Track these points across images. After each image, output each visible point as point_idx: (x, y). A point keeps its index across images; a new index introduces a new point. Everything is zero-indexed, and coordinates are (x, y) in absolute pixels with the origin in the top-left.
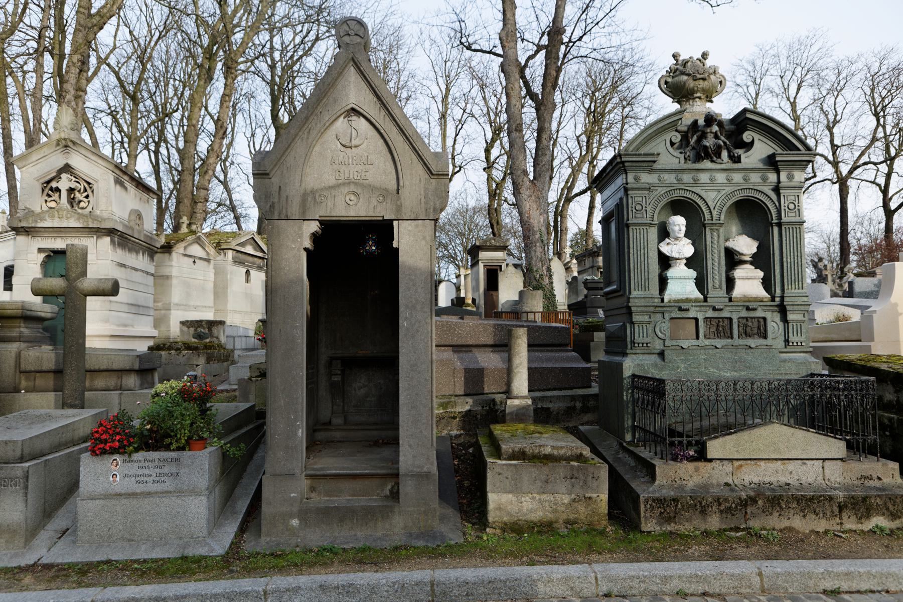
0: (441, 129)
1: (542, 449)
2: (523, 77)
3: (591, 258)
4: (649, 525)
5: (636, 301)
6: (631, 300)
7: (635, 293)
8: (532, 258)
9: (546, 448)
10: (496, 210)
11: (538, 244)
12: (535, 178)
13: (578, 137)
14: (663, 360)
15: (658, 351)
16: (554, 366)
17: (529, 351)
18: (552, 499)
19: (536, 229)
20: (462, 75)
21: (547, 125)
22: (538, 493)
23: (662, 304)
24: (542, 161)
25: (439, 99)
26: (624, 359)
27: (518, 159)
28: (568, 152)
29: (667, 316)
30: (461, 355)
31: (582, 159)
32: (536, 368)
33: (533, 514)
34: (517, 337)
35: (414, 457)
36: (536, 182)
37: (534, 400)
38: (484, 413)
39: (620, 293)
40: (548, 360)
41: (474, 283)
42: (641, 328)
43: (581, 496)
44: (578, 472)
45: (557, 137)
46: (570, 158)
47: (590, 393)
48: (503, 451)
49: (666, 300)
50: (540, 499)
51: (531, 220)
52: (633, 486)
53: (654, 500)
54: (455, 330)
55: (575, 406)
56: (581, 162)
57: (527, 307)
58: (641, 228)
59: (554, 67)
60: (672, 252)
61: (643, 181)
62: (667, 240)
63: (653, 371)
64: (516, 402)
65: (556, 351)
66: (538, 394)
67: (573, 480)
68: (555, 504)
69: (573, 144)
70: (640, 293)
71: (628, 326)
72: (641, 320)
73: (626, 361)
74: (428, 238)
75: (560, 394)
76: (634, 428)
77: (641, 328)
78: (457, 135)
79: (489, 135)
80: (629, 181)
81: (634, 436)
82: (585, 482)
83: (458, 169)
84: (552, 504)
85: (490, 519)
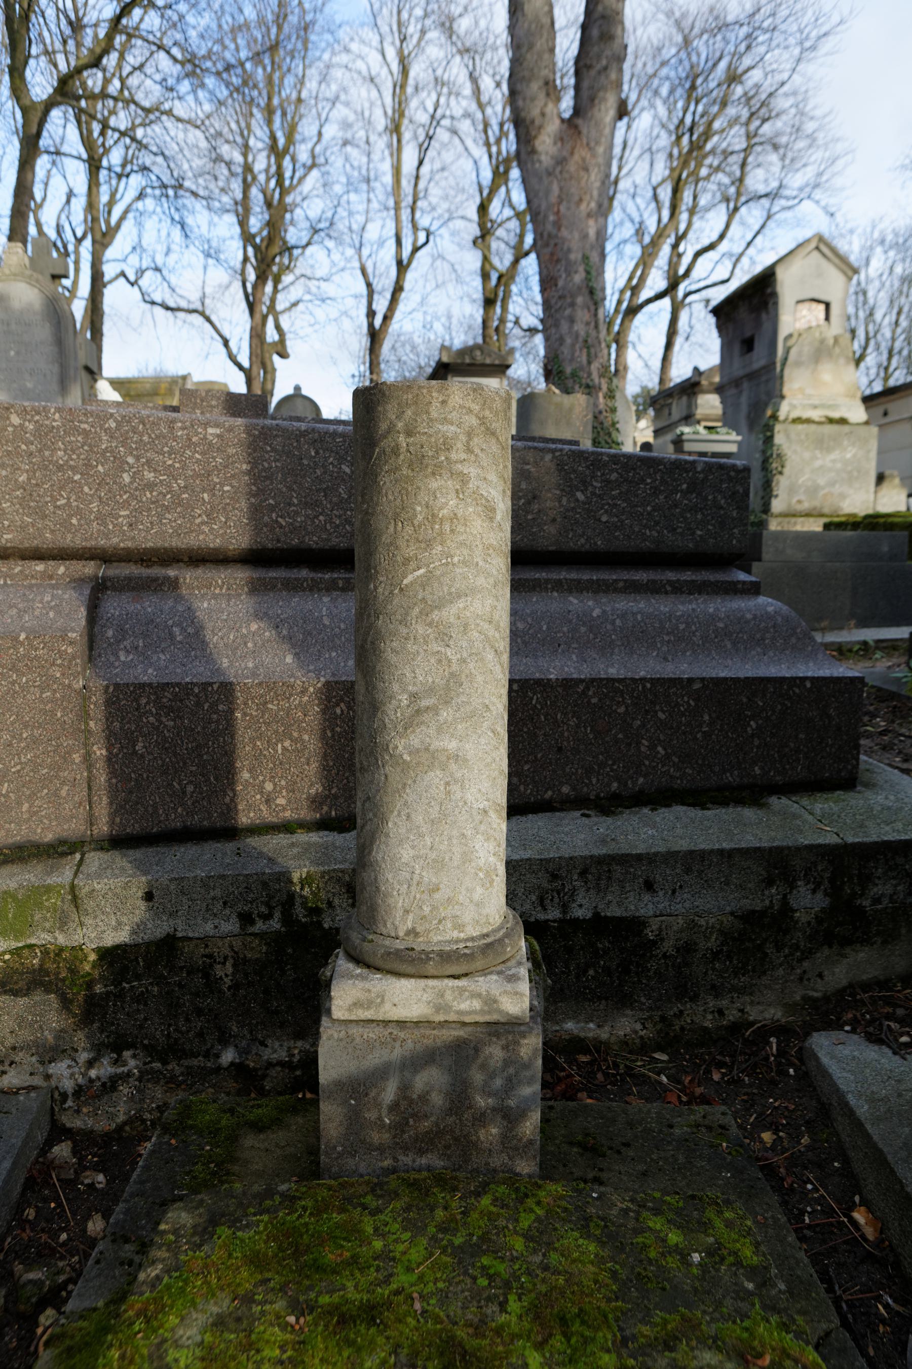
0: (392, 155)
8: (561, 340)
11: (580, 300)
13: (655, 189)
17: (517, 587)
19: (575, 256)
20: (433, 35)
24: (599, 57)
27: (531, 46)
30: (299, 604)
32: (568, 684)
34: (418, 462)
36: (579, 122)
38: (257, 951)
46: (640, 232)
51: (564, 233)
54: (121, 465)
55: (786, 910)
65: (678, 589)
78: (421, 163)
79: (487, 175)
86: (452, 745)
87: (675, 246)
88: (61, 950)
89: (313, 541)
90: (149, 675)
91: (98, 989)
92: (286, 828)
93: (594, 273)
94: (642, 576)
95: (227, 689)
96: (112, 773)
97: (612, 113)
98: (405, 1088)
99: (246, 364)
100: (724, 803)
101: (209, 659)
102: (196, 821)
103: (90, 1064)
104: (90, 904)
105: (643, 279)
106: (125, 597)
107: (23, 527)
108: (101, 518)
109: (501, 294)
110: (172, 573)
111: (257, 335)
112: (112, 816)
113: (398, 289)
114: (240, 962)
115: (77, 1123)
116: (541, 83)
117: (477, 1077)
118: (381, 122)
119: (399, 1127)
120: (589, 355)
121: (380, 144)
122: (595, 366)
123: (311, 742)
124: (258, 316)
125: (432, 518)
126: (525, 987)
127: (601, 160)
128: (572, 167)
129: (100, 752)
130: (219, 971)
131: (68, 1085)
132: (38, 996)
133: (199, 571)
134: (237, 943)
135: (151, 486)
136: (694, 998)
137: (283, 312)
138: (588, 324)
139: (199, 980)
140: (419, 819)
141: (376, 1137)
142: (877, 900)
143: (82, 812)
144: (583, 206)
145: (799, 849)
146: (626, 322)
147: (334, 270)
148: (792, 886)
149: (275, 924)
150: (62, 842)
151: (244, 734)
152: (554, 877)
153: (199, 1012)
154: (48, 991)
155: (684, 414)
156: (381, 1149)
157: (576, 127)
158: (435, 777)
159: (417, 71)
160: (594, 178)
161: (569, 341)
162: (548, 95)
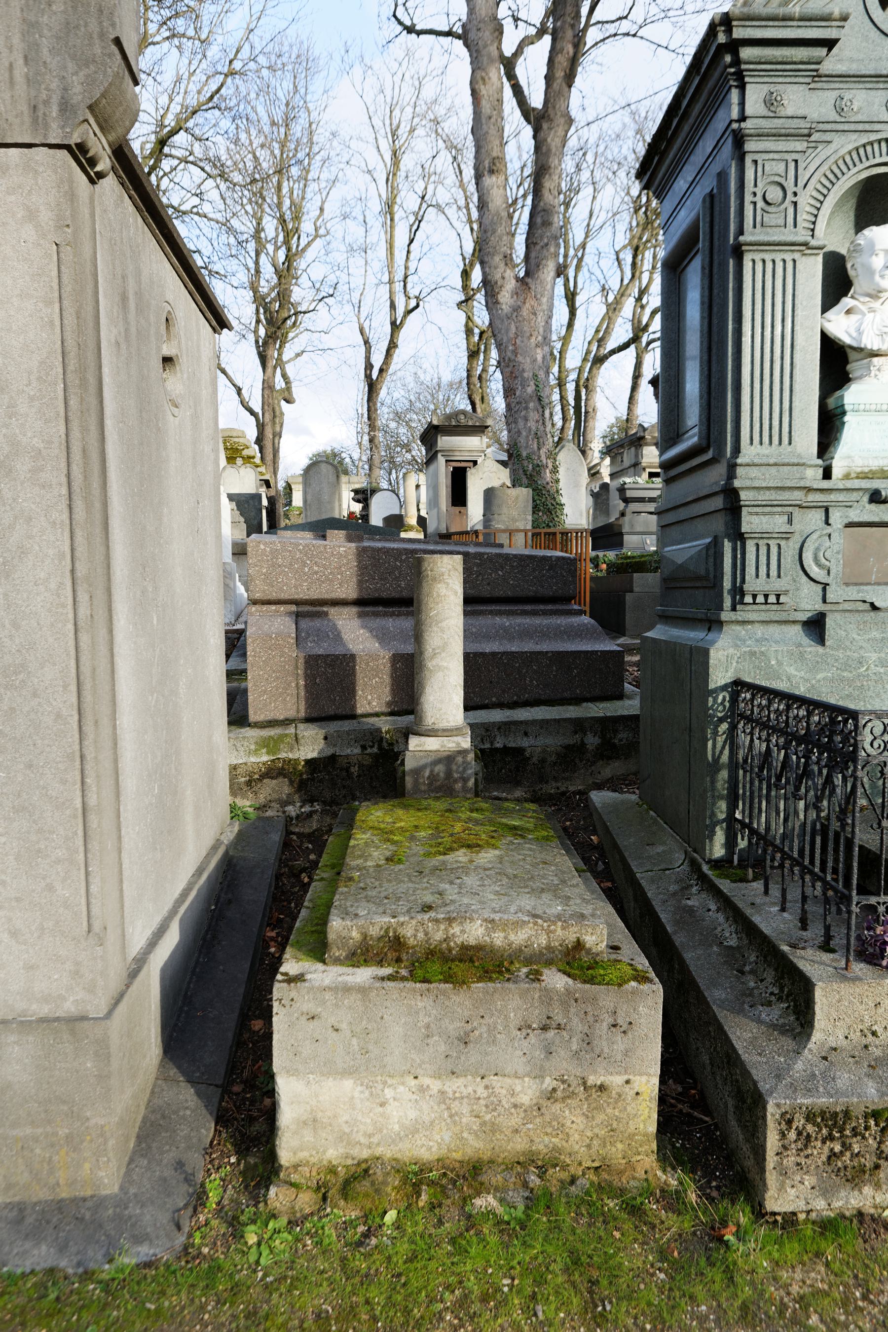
0: (386, 232)
1: (456, 929)
2: (511, 76)
3: (633, 449)
4: (792, 1192)
5: (754, 472)
6: (740, 471)
7: (749, 452)
9: (467, 926)
10: (480, 377)
11: (531, 405)
12: (527, 273)
13: (617, 253)
14: (821, 639)
15: (804, 617)
16: (538, 648)
17: (466, 614)
18: (481, 1092)
19: (528, 374)
20: (420, 132)
21: (553, 162)
22: (437, 1076)
23: (826, 484)
24: (542, 237)
25: (381, 177)
26: (711, 636)
27: (494, 231)
28: (601, 277)
29: (837, 517)
31: (622, 293)
32: (494, 654)
33: (420, 1139)
34: (434, 579)
35: (30, 968)
36: (529, 280)
37: (480, 732)
38: (368, 761)
39: (709, 455)
40: (525, 634)
41: (431, 492)
42: (763, 551)
43: (574, 1083)
44: (566, 1011)
45: (583, 255)
47: (620, 712)
48: (331, 936)
49: (837, 471)
50: (442, 1093)
51: (520, 358)
52: (739, 1045)
53: (810, 1117)
54: (304, 564)
55: (583, 744)
56: (622, 295)
57: (498, 523)
58: (778, 257)
59: (569, 34)
60: (860, 332)
61: (790, 111)
62: (847, 302)
63: (792, 670)
64: (432, 744)
65: (545, 613)
66: (497, 716)
67: (551, 1034)
68: (492, 1107)
69: (608, 263)
70: (765, 450)
71: (727, 546)
72: (766, 527)
73: (720, 643)
74: (46, 216)
75: (548, 717)
76: (732, 827)
77: (763, 551)
78: (411, 241)
80: (749, 111)
81: (730, 843)
82: (588, 1040)
83: (413, 303)
84: (480, 1107)
85: (285, 1156)
86: (445, 664)
87: (639, 299)
88: (290, 760)
89: (384, 595)
90: (321, 652)
91: (305, 776)
92: (377, 715)
93: (541, 386)
94: (528, 607)
95: (353, 657)
96: (307, 691)
97: (552, 274)
98: (432, 771)
99: (257, 408)
100: (563, 705)
101: (344, 645)
102: (340, 712)
103: (301, 807)
104: (302, 741)
105: (607, 332)
106: (307, 620)
107: (264, 591)
108: (296, 587)
109: (483, 347)
110: (325, 609)
111: (268, 386)
112: (306, 709)
113: (392, 346)
114: (361, 766)
115: (297, 830)
116: (501, 257)
117: (454, 767)
118: (375, 206)
119: (430, 784)
120: (538, 444)
121: (376, 224)
122: (543, 451)
123: (387, 679)
124: (269, 370)
125: (439, 596)
126: (469, 739)
127: (545, 307)
128: (525, 312)
129: (302, 682)
130: (352, 770)
131: (293, 814)
132: (281, 779)
133: (337, 608)
134: (360, 758)
135: (316, 573)
136: (547, 782)
137: (289, 361)
138: (537, 421)
139: (344, 774)
140: (435, 687)
141: (423, 788)
142: (621, 740)
143: (295, 707)
144: (533, 340)
145: (587, 719)
146: (594, 371)
147: (333, 324)
148: (585, 734)
149: (375, 750)
150: (287, 720)
151: (360, 675)
152: (487, 730)
153: (344, 787)
154: (285, 777)
155: (633, 462)
156: (425, 792)
157: (527, 284)
158: (440, 674)
159: (407, 162)
160: (541, 320)
161: (524, 434)
162: (506, 264)
